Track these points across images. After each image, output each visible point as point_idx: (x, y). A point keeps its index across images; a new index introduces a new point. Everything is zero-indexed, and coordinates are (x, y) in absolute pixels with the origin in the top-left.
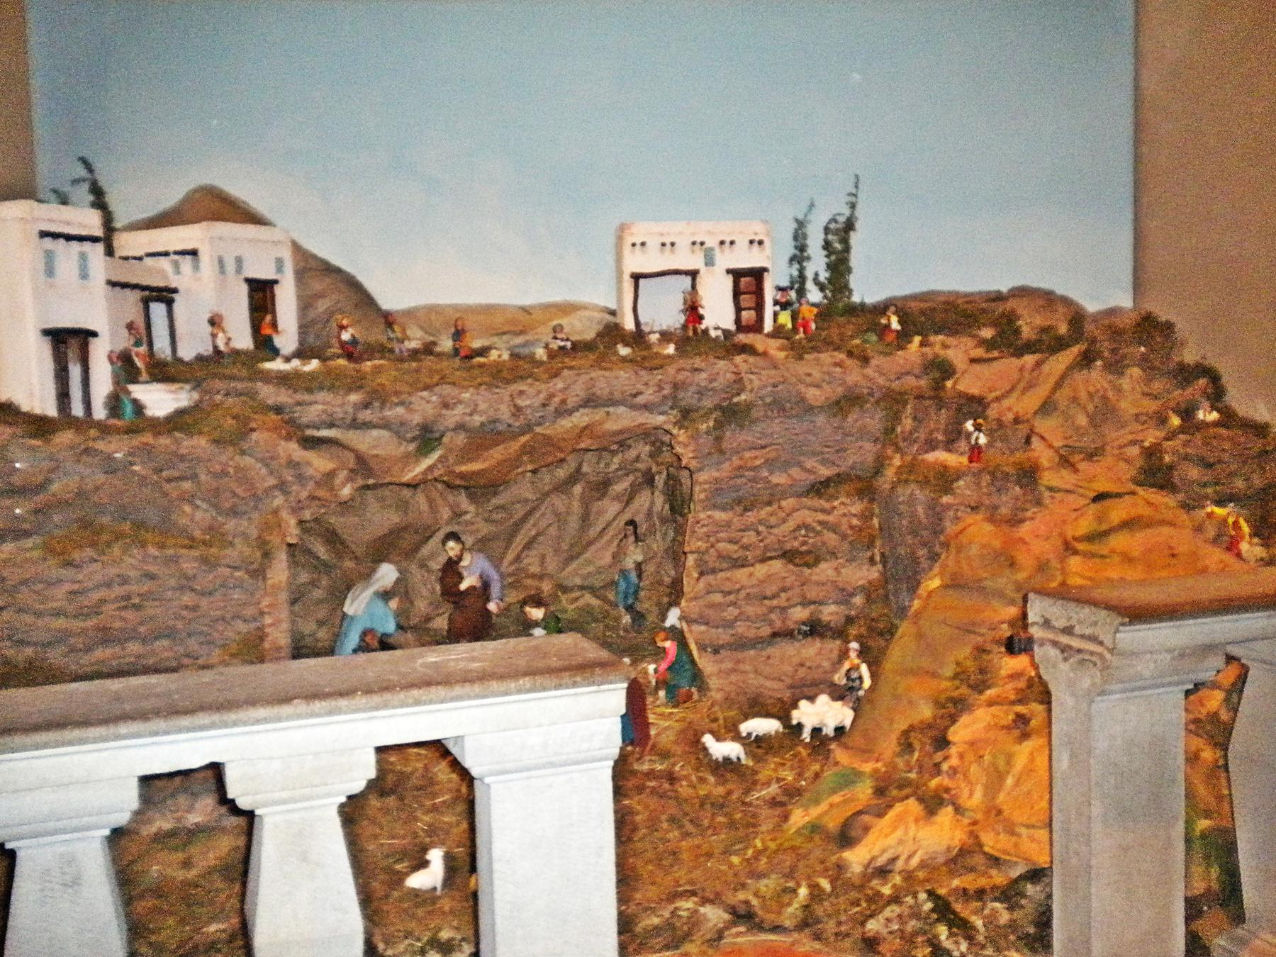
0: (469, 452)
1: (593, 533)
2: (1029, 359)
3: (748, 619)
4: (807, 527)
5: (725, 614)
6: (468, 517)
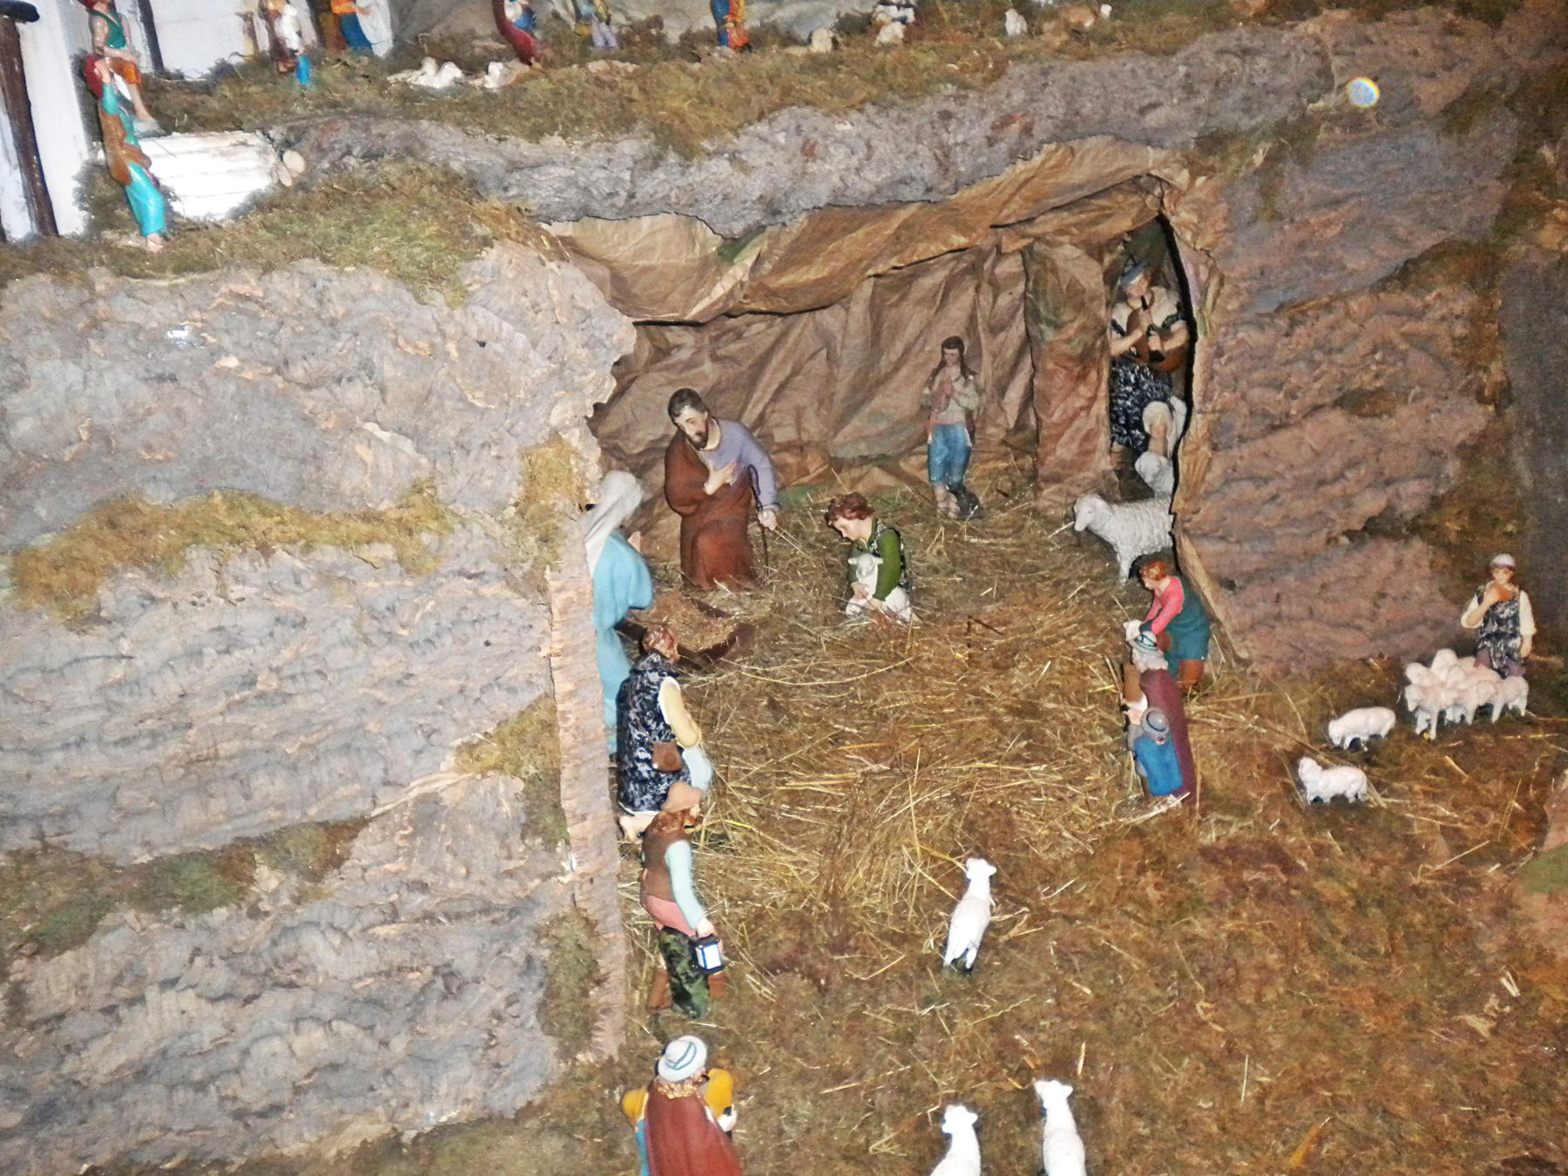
0: (798, 254)
1: (884, 364)
3: (1295, 522)
4: (1387, 345)
5: (1258, 519)
6: (684, 355)
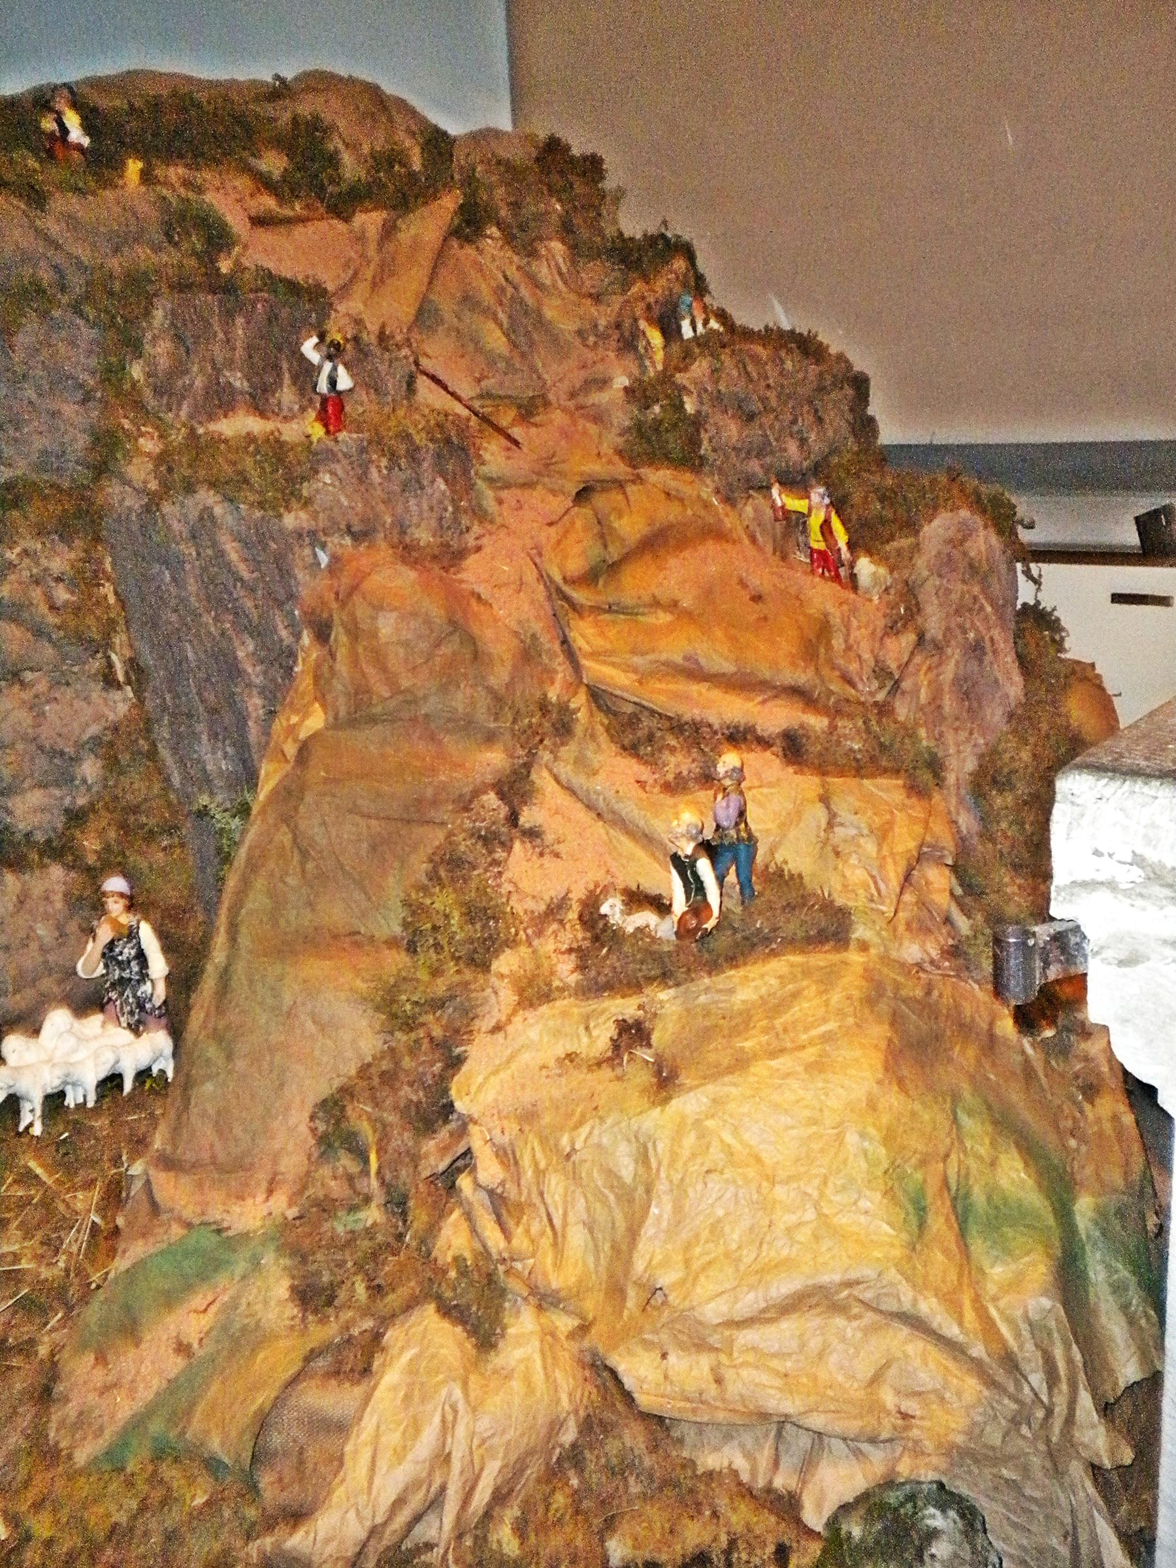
2: (370, 221)
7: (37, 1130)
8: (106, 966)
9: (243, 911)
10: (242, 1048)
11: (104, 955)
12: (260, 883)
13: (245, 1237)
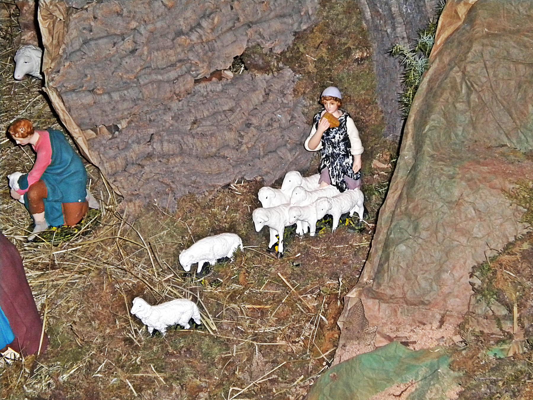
7: (280, 249)
8: (324, 144)
9: (427, 127)
10: (425, 222)
11: (323, 137)
12: (439, 106)
13: (426, 352)
